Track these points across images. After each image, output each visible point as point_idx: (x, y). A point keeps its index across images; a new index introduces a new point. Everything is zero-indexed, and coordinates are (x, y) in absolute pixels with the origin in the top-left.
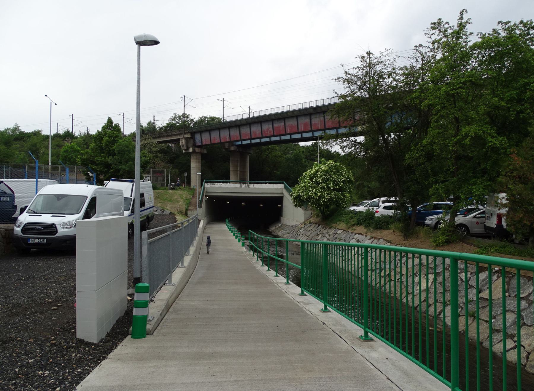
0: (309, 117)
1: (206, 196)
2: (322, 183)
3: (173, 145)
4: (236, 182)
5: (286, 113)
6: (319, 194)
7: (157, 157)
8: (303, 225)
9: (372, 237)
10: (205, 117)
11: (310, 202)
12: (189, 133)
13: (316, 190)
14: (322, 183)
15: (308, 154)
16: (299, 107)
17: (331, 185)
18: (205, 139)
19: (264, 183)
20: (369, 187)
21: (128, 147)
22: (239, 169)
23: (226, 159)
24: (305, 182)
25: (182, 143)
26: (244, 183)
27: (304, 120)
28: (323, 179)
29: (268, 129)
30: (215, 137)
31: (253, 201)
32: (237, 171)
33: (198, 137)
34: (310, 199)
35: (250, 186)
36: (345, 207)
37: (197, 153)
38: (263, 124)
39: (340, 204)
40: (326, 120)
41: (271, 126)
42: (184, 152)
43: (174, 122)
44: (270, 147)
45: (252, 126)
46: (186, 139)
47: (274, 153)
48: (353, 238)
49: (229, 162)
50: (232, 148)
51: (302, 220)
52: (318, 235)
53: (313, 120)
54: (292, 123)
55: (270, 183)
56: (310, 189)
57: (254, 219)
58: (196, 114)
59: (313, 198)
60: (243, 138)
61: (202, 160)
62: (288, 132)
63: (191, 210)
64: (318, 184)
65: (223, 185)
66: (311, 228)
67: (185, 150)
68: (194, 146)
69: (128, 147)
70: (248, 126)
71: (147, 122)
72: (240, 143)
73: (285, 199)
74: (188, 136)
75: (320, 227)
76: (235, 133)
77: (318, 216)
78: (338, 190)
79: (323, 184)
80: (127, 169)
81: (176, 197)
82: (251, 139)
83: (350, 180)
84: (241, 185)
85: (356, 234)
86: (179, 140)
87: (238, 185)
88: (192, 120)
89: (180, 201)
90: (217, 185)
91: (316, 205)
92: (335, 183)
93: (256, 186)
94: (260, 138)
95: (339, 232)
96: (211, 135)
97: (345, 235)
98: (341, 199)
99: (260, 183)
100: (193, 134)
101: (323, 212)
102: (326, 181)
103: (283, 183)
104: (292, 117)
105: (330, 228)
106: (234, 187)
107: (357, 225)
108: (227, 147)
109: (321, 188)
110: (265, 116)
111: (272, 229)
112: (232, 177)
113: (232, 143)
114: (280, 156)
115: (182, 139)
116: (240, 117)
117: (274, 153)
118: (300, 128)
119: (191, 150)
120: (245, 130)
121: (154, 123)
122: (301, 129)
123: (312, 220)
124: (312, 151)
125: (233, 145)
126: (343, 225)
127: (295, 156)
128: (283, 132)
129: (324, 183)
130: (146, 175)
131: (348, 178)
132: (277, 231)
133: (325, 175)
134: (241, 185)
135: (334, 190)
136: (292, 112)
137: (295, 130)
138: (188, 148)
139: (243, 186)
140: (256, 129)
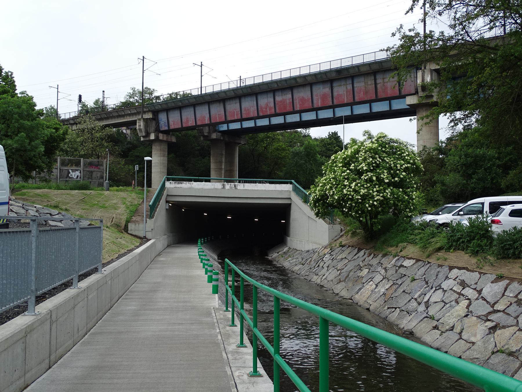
0: (329, 85)
1: (167, 202)
2: (367, 171)
3: (129, 132)
4: (219, 181)
5: (295, 79)
6: (363, 191)
7: (101, 146)
8: (327, 250)
9: (500, 278)
10: (177, 94)
11: (345, 207)
12: (149, 111)
13: (356, 185)
14: (367, 171)
15: (324, 149)
16: (315, 70)
17: (385, 175)
18: (174, 120)
19: (260, 182)
20: (443, 184)
21: (19, 107)
22: (223, 167)
23: (205, 154)
24: (335, 172)
25: (140, 126)
26: (228, 181)
28: (369, 164)
30: (189, 117)
31: (245, 211)
32: (221, 169)
33: (162, 117)
34: (346, 202)
35: (239, 188)
36: (411, 217)
37: (162, 141)
38: (259, 97)
39: (400, 211)
40: (356, 89)
41: (272, 100)
42: (142, 139)
43: (131, 100)
44: (270, 134)
45: (243, 100)
46: (146, 121)
47: (276, 145)
48: (447, 278)
49: (210, 157)
50: (214, 136)
51: (326, 242)
52: (360, 269)
53: (335, 90)
54: (303, 94)
55: (271, 183)
56: (346, 183)
57: (244, 239)
58: (163, 88)
59: (352, 200)
60: (229, 118)
62: (298, 108)
63: (135, 222)
64: (360, 173)
65: (196, 185)
66: (343, 255)
67: (143, 137)
68: (158, 130)
69: (19, 107)
70: (238, 101)
71: (94, 100)
72: (224, 127)
73: (293, 207)
74: (149, 116)
75: (362, 253)
76: (217, 111)
77: (354, 234)
78: (396, 185)
79: (370, 174)
80: (15, 146)
81: (115, 201)
82: (241, 120)
83: (418, 168)
84: (224, 185)
85: (451, 268)
86: (134, 123)
87: (218, 185)
88: (158, 98)
89: (119, 208)
90: (186, 185)
91: (357, 212)
92: (393, 171)
93: (249, 186)
94: (254, 119)
95: (407, 263)
97: (423, 270)
98: (403, 201)
99: (255, 182)
100: (156, 113)
101: (364, 226)
102: (375, 168)
103: (291, 183)
104: (303, 85)
105: (384, 256)
106: (213, 187)
107: (448, 249)
108: (206, 134)
109: (366, 181)
110: (263, 84)
111: (273, 256)
112: (213, 174)
113: (213, 126)
114: (284, 149)
115: (140, 120)
116: (225, 87)
117: (276, 145)
118: (315, 102)
119: (152, 137)
120: (233, 107)
121: (103, 102)
122: (318, 103)
123: (344, 240)
124: (329, 144)
125: (215, 131)
126: (412, 250)
127: (306, 148)
128: (289, 109)
129: (371, 171)
130: (74, 168)
131: (414, 164)
132: (282, 259)
133: (374, 158)
134: (224, 185)
135: (389, 184)
136: (304, 77)
137: (308, 105)
138: (148, 134)
139: (228, 186)
140: (249, 104)
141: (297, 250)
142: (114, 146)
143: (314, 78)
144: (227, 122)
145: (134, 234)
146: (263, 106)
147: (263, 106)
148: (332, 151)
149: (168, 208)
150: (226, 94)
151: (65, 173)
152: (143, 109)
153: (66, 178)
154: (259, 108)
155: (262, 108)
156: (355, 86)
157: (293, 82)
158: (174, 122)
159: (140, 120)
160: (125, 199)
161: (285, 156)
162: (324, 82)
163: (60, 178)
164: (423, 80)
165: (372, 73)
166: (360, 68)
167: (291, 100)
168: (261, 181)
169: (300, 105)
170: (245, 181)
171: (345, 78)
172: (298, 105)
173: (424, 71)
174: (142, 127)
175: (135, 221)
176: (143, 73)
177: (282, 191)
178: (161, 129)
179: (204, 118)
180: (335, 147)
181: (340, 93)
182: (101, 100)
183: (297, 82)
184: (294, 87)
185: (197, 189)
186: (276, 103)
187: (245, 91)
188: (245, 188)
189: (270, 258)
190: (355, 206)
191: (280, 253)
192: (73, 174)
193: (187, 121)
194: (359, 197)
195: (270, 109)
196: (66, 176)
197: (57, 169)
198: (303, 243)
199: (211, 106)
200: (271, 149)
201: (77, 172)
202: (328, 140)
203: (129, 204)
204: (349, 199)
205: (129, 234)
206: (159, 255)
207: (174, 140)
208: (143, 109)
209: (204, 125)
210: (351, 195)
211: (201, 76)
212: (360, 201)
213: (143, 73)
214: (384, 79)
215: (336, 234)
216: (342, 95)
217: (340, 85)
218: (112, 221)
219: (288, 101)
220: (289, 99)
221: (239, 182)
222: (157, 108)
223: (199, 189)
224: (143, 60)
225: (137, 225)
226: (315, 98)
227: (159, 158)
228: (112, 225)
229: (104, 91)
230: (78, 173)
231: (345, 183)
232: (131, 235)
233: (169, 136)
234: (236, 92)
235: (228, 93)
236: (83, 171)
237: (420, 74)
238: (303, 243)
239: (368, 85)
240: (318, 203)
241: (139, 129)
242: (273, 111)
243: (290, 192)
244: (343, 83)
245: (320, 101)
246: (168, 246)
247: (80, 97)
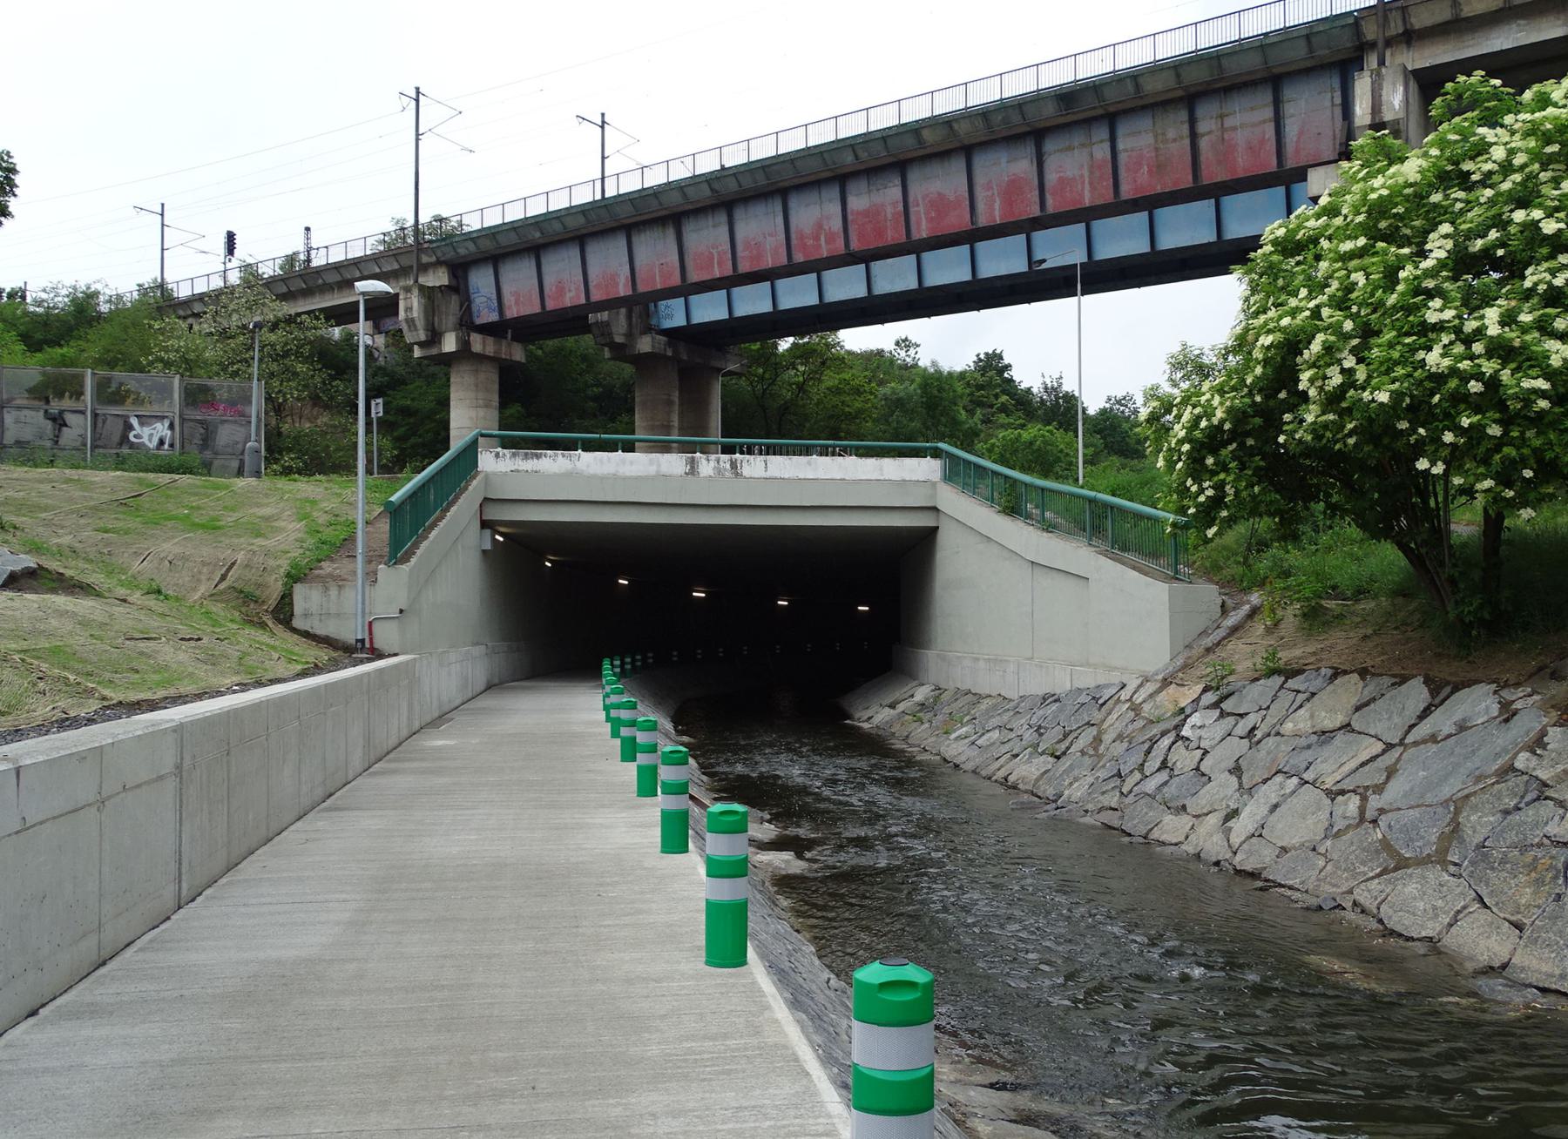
0: (1030, 149)
4: (665, 448)
12: (439, 263)
18: (519, 290)
25: (409, 309)
27: (1004, 170)
29: (819, 226)
33: (481, 282)
35: (747, 471)
37: (481, 358)
38: (794, 202)
40: (1123, 158)
45: (739, 213)
49: (631, 411)
50: (645, 345)
53: (1051, 163)
54: (940, 185)
57: (768, 660)
61: (503, 405)
62: (922, 231)
65: (588, 461)
67: (421, 345)
68: (467, 324)
74: (438, 278)
76: (656, 256)
81: (267, 511)
84: (692, 462)
87: (674, 463)
90: (553, 463)
96: (545, 269)
99: (807, 451)
100: (459, 269)
103: (936, 454)
104: (943, 155)
106: (652, 470)
108: (619, 339)
111: (875, 714)
113: (641, 304)
114: (858, 392)
118: (981, 206)
119: (450, 344)
122: (991, 211)
124: (980, 387)
134: (692, 462)
138: (434, 337)
139: (707, 465)
141: (980, 698)
142: (333, 378)
143: (979, 123)
144: (687, 290)
145: (320, 631)
146: (807, 231)
147: (807, 231)
148: (991, 406)
149: (488, 546)
150: (684, 195)
151: (113, 429)
152: (418, 259)
153: (120, 444)
154: (793, 236)
155: (802, 237)
156: (1121, 146)
157: (910, 141)
158: (517, 294)
159: (408, 290)
160: (314, 502)
161: (860, 412)
162: (1011, 139)
163: (94, 447)
164: (1376, 108)
165: (1181, 99)
166: (1141, 80)
167: (901, 207)
168: (827, 447)
169: (930, 220)
170: (768, 447)
171: (1088, 122)
172: (924, 223)
173: (1379, 74)
174: (415, 314)
175: (331, 576)
176: (417, 140)
177: (903, 482)
178: (478, 321)
179: (613, 278)
180: (997, 396)
181: (1069, 174)
182: (302, 257)
183: (921, 141)
184: (911, 161)
185: (594, 477)
186: (850, 217)
187: (747, 182)
188: (768, 474)
189: (866, 726)
190: (1499, 444)
191: (901, 707)
192: (146, 431)
193: (561, 291)
194: (1542, 384)
195: (830, 239)
196: (116, 438)
197: (83, 413)
198: (1012, 668)
199: (635, 239)
200: (816, 392)
201: (159, 425)
202: (978, 375)
203: (323, 519)
204: (1461, 399)
205: (295, 630)
206: (438, 720)
207: (518, 354)
208: (418, 259)
209: (611, 304)
210: (1479, 376)
211: (603, 158)
212: (1543, 404)
213: (417, 140)
214: (1222, 117)
215: (1201, 623)
216: (1074, 179)
217: (1070, 148)
218: (223, 577)
219: (889, 210)
220: (894, 204)
221: (750, 452)
222: (462, 251)
223: (603, 479)
224: (417, 101)
225: (333, 592)
226: (980, 194)
227: (473, 413)
228: (222, 593)
229: (308, 229)
230: (161, 429)
231: (1432, 317)
232: (306, 635)
233: (504, 342)
234: (716, 186)
235: (690, 192)
236: (183, 420)
237: (1362, 87)
238: (1012, 668)
239: (1165, 141)
240: (1214, 451)
241: (407, 320)
242: (840, 243)
243: (934, 484)
244: (1077, 138)
245: (997, 205)
246: (490, 687)
247: (231, 237)
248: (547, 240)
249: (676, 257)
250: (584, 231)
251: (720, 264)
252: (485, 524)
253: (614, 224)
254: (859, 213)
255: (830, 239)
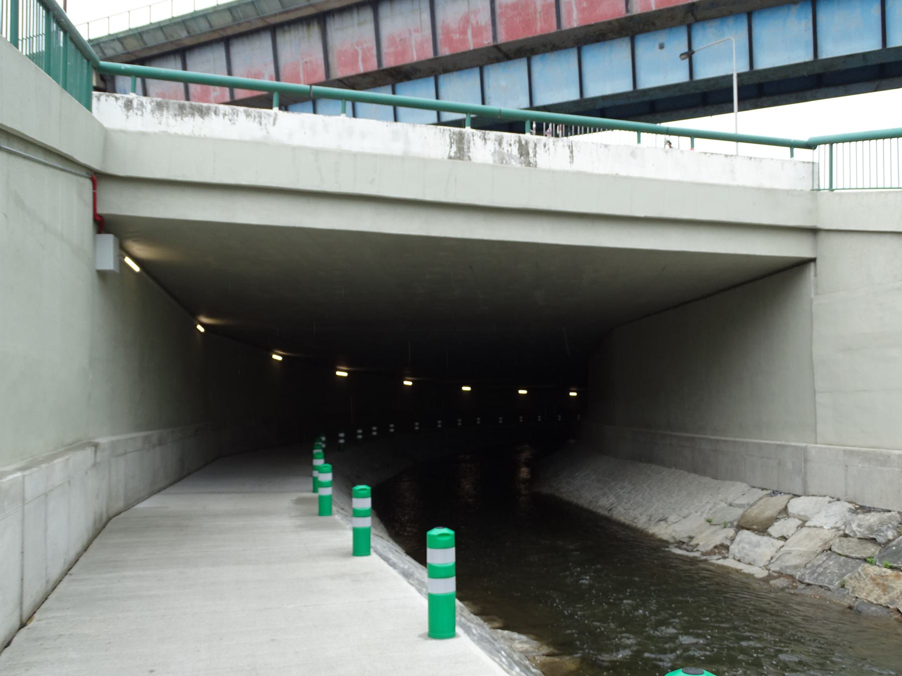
29: (466, 20)
106: (397, 149)
154: (439, 31)
155: (448, 32)
169: (582, 11)
186: (498, 11)
248: (194, 41)
249: (321, 55)
250: (229, 32)
251: (364, 61)
252: (102, 224)
253: (260, 24)
254: (507, 6)
255: (478, 32)
